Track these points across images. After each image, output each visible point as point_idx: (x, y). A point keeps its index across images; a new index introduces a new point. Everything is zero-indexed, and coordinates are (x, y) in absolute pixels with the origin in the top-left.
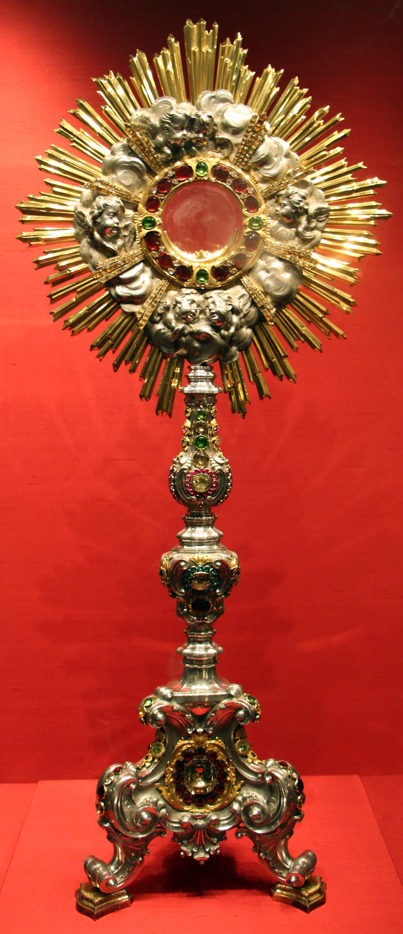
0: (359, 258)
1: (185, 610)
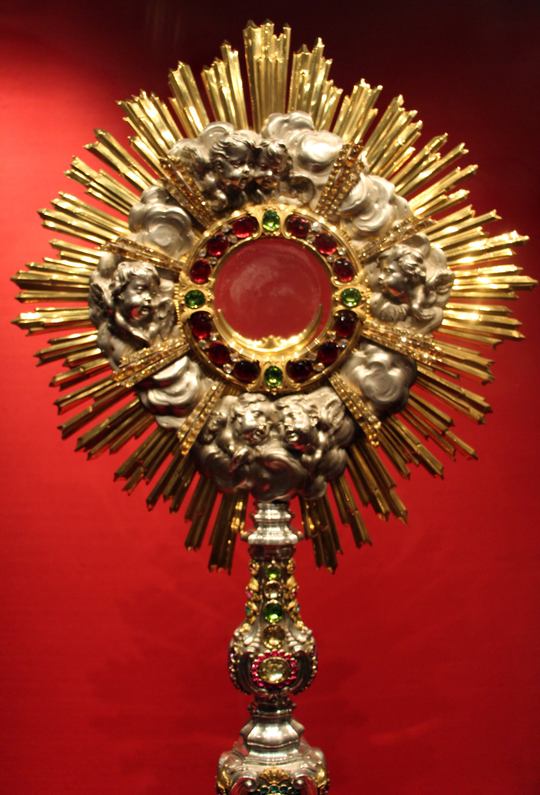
0: (495, 345)
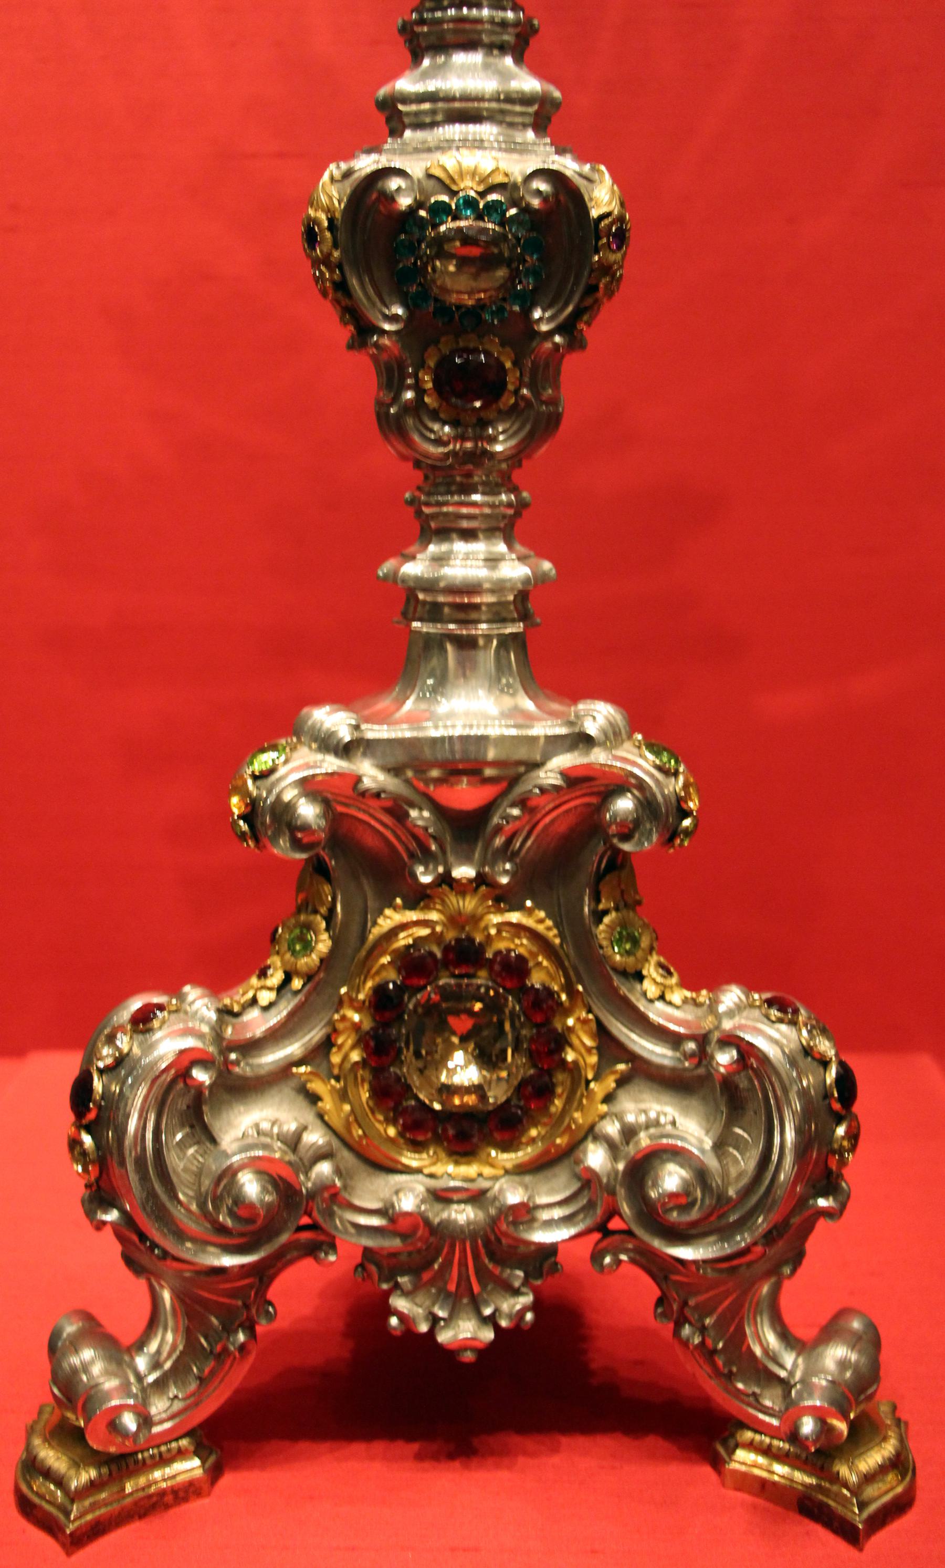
1: (409, 395)
